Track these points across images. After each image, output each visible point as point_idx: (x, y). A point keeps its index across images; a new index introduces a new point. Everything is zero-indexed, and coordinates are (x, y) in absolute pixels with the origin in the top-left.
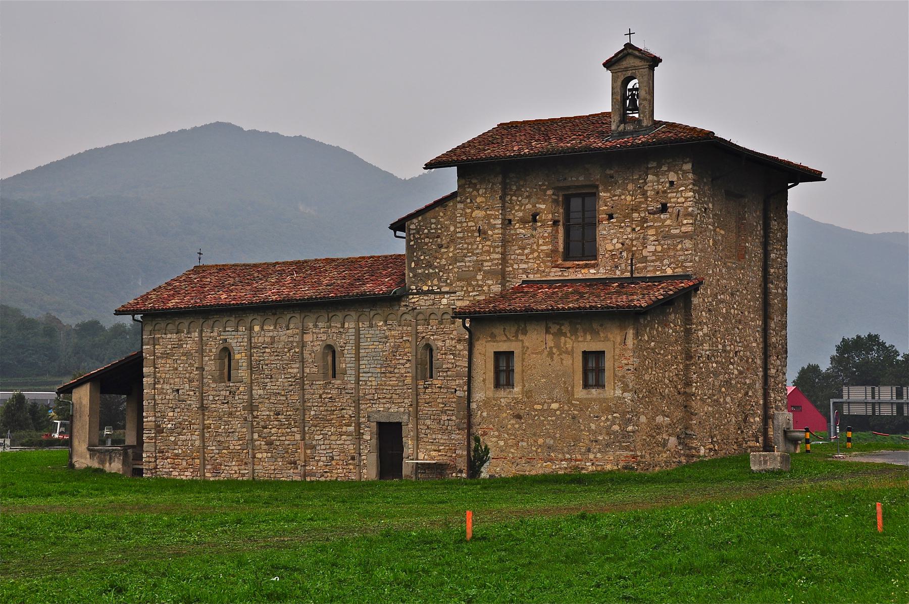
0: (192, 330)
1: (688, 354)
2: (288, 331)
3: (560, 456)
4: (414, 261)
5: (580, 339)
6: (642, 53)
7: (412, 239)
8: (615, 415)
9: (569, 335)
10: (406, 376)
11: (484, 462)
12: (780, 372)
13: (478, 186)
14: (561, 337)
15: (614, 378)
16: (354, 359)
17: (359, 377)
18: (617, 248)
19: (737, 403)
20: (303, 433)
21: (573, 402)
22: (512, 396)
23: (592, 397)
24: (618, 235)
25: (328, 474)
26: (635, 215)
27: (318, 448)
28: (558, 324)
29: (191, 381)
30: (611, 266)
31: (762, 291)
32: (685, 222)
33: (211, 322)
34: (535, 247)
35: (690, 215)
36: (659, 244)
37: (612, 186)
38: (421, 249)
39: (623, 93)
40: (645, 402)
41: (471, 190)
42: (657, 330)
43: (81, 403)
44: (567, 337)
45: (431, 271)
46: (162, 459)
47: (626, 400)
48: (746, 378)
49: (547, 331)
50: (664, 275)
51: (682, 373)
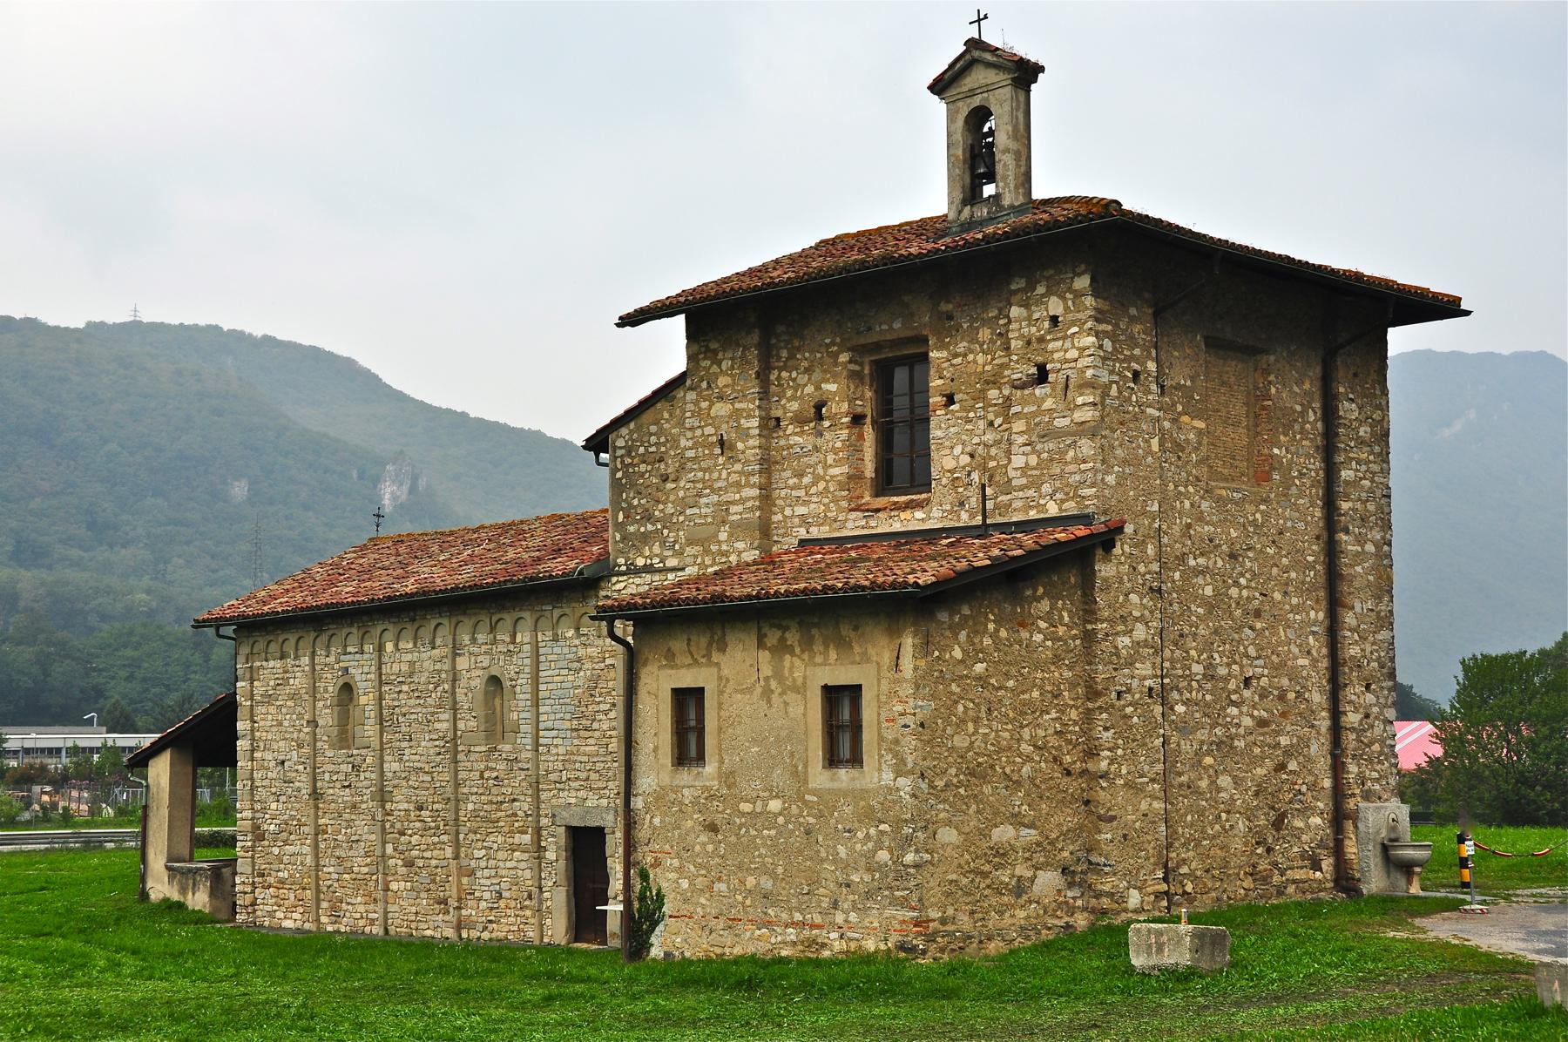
0: (301, 652)
1: (1091, 687)
2: (434, 651)
3: (784, 916)
4: (622, 509)
5: (819, 659)
6: (998, 56)
7: (619, 466)
8: (882, 827)
9: (798, 650)
10: (611, 737)
11: (655, 924)
12: (1376, 718)
13: (720, 355)
14: (784, 654)
15: (879, 744)
16: (529, 703)
17: (537, 737)
18: (962, 464)
19: (1254, 789)
20: (457, 845)
21: (807, 797)
22: (701, 784)
23: (840, 786)
24: (964, 437)
25: (494, 925)
26: (993, 393)
27: (479, 874)
28: (779, 627)
29: (300, 746)
30: (951, 504)
31: (1322, 549)
32: (1080, 401)
33: (324, 637)
34: (820, 471)
35: (1091, 385)
36: (1034, 451)
37: (951, 336)
38: (633, 485)
39: (970, 142)
40: (955, 796)
41: (709, 362)
42: (995, 636)
43: (159, 784)
44: (796, 656)
45: (650, 527)
46: (263, 887)
47: (902, 793)
48: (1278, 733)
49: (761, 645)
50: (1042, 516)
51: (1077, 728)
